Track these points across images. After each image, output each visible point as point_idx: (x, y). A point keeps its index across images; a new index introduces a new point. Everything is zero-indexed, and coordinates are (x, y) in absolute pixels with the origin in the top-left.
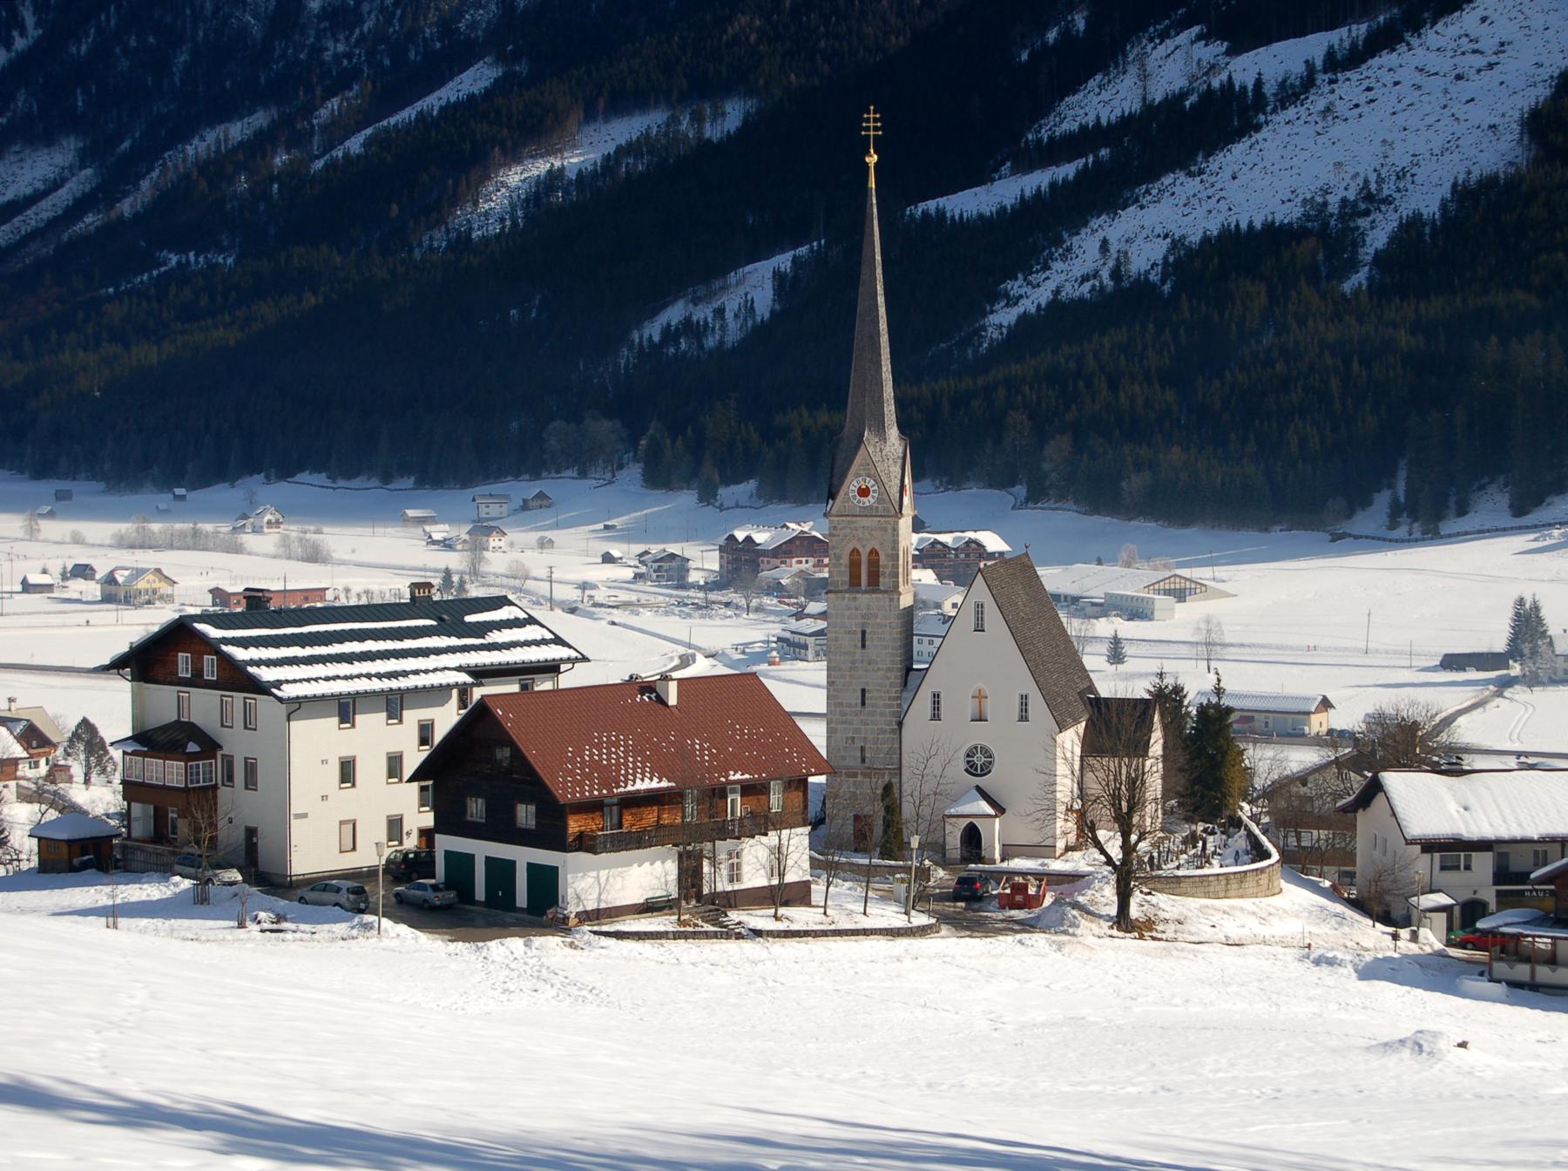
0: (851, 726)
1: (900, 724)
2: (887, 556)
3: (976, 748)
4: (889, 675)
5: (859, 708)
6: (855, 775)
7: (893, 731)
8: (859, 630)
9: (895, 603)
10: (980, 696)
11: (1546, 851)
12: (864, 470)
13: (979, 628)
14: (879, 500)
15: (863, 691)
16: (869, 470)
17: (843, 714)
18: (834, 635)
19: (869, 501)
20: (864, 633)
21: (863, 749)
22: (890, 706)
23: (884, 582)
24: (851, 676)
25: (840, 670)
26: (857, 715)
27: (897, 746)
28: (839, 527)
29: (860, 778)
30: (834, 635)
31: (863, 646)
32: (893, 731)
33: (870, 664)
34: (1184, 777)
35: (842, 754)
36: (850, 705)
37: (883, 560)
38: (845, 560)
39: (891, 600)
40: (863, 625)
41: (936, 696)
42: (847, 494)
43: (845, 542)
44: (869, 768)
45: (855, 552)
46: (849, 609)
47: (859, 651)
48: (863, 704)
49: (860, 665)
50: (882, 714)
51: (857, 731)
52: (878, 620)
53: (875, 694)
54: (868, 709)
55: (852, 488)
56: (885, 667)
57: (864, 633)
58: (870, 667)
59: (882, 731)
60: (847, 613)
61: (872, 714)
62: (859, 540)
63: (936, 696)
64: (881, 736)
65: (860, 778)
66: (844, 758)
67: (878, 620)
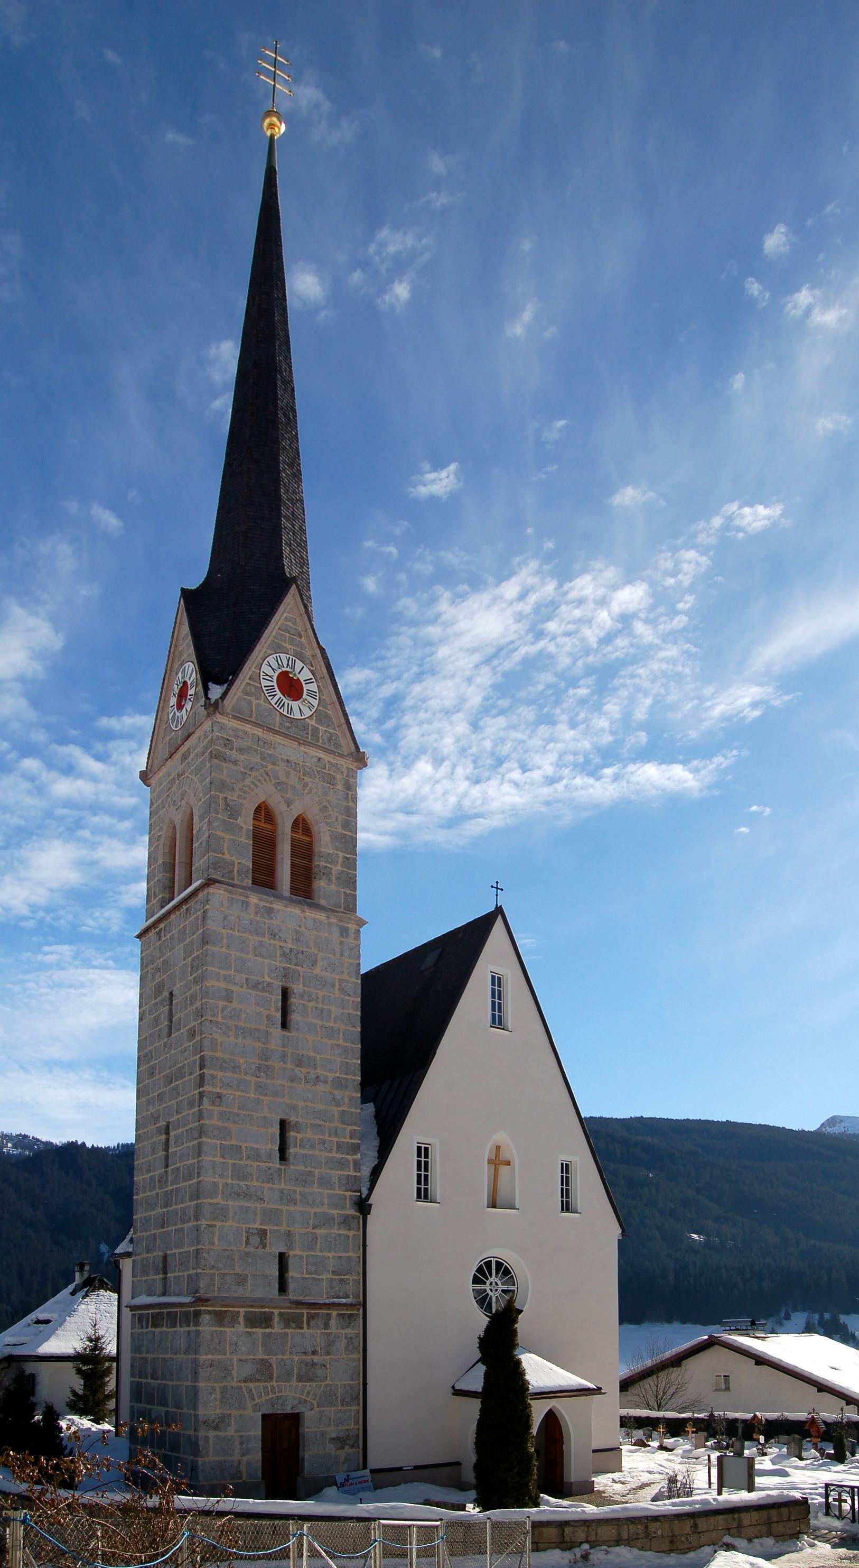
0: (259, 1206)
1: (363, 1207)
2: (335, 836)
3: (488, 1264)
4: (338, 1094)
5: (276, 1164)
6: (266, 1321)
7: (346, 1221)
8: (278, 984)
9: (351, 940)
10: (498, 1161)
11: (142, 1327)
12: (292, 642)
13: (498, 1021)
14: (320, 715)
15: (283, 1124)
16: (301, 645)
17: (241, 1174)
18: (222, 985)
19: (299, 710)
20: (285, 994)
21: (283, 1259)
22: (341, 1164)
23: (321, 885)
24: (258, 1086)
25: (236, 1068)
26: (270, 1179)
27: (356, 1254)
28: (237, 743)
29: (277, 1328)
30: (222, 985)
31: (284, 1025)
32: (346, 1221)
33: (299, 1065)
34: (193, 1347)
35: (238, 1269)
36: (256, 1156)
37: (324, 844)
38: (246, 822)
39: (344, 932)
40: (286, 974)
41: (423, 1151)
42: (256, 678)
43: (248, 781)
44: (299, 1304)
45: (264, 813)
46: (256, 932)
47: (277, 1031)
48: (283, 1157)
49: (278, 1065)
50: (325, 1182)
51: (272, 1216)
52: (317, 971)
53: (309, 1135)
54: (294, 1168)
55: (265, 668)
56: (331, 1076)
57: (285, 994)
58: (300, 1072)
59: (327, 1221)
60: (254, 940)
61: (304, 1179)
62: (281, 786)
63: (423, 1151)
64: (320, 1232)
65: (277, 1328)
66: (241, 1280)
67: (317, 971)
